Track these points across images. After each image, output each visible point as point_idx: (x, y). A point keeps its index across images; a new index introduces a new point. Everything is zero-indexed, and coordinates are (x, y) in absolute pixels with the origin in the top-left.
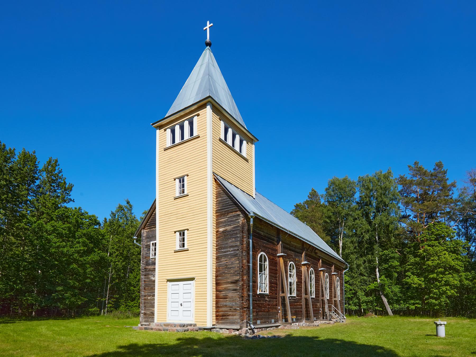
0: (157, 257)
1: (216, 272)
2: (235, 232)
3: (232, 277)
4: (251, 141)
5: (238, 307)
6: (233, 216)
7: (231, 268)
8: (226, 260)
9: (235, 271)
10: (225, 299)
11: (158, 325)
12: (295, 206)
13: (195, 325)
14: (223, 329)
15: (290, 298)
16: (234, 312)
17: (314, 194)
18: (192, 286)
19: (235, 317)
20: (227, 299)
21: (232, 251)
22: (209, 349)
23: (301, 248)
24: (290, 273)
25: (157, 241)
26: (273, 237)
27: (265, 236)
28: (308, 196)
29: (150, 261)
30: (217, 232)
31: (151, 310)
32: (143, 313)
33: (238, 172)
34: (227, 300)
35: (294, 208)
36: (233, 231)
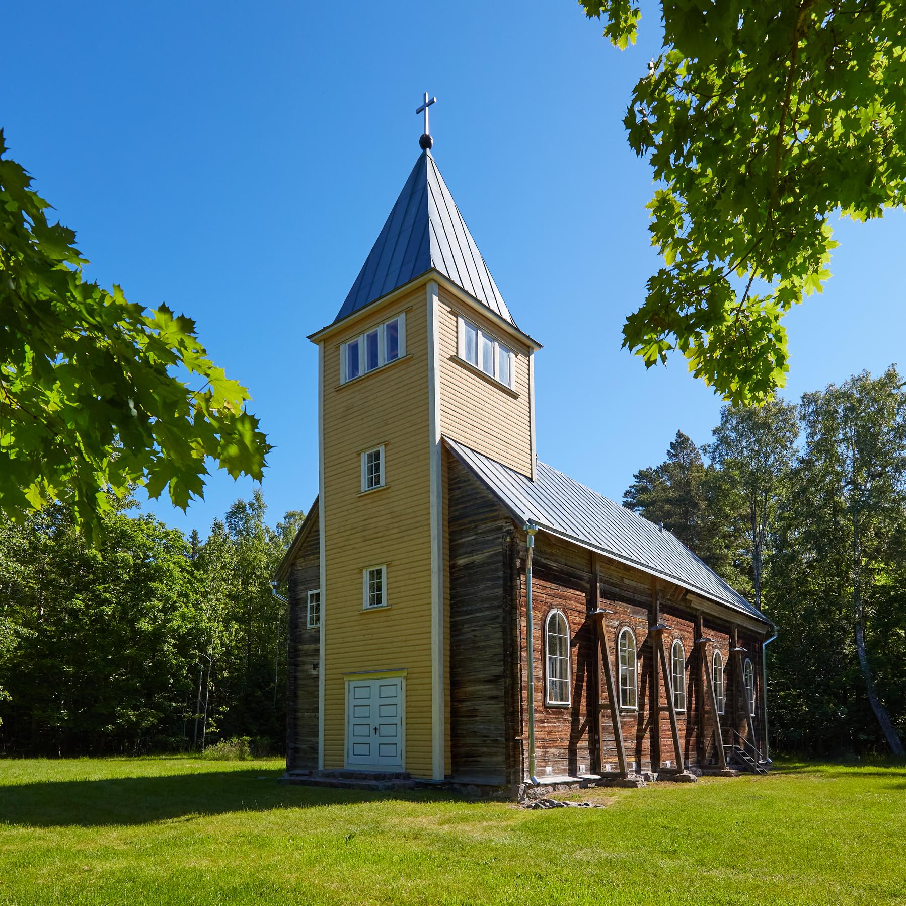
0: (322, 624)
1: (451, 657)
2: (493, 567)
3: (487, 669)
4: (524, 351)
5: (501, 737)
6: (489, 531)
7: (484, 647)
8: (474, 630)
9: (495, 655)
10: (471, 719)
11: (328, 775)
12: (635, 476)
13: (407, 776)
14: (468, 784)
15: (623, 714)
16: (494, 747)
17: (681, 444)
18: (399, 688)
19: (495, 759)
20: (477, 718)
21: (487, 609)
22: (446, 827)
23: (649, 592)
24: (624, 654)
25: (322, 591)
26: (579, 573)
27: (561, 571)
28: (669, 453)
29: (307, 635)
30: (452, 567)
31: (311, 741)
32: (292, 749)
33: (501, 427)
34: (476, 721)
35: (633, 481)
36: (489, 564)
